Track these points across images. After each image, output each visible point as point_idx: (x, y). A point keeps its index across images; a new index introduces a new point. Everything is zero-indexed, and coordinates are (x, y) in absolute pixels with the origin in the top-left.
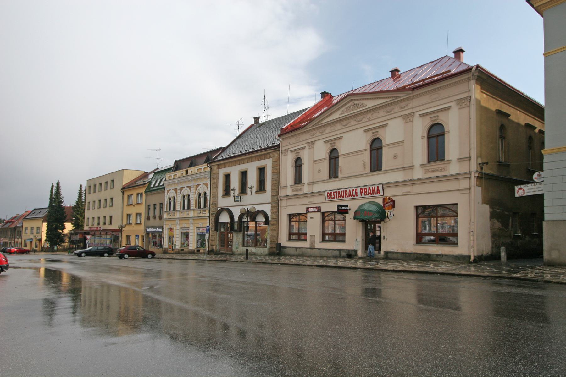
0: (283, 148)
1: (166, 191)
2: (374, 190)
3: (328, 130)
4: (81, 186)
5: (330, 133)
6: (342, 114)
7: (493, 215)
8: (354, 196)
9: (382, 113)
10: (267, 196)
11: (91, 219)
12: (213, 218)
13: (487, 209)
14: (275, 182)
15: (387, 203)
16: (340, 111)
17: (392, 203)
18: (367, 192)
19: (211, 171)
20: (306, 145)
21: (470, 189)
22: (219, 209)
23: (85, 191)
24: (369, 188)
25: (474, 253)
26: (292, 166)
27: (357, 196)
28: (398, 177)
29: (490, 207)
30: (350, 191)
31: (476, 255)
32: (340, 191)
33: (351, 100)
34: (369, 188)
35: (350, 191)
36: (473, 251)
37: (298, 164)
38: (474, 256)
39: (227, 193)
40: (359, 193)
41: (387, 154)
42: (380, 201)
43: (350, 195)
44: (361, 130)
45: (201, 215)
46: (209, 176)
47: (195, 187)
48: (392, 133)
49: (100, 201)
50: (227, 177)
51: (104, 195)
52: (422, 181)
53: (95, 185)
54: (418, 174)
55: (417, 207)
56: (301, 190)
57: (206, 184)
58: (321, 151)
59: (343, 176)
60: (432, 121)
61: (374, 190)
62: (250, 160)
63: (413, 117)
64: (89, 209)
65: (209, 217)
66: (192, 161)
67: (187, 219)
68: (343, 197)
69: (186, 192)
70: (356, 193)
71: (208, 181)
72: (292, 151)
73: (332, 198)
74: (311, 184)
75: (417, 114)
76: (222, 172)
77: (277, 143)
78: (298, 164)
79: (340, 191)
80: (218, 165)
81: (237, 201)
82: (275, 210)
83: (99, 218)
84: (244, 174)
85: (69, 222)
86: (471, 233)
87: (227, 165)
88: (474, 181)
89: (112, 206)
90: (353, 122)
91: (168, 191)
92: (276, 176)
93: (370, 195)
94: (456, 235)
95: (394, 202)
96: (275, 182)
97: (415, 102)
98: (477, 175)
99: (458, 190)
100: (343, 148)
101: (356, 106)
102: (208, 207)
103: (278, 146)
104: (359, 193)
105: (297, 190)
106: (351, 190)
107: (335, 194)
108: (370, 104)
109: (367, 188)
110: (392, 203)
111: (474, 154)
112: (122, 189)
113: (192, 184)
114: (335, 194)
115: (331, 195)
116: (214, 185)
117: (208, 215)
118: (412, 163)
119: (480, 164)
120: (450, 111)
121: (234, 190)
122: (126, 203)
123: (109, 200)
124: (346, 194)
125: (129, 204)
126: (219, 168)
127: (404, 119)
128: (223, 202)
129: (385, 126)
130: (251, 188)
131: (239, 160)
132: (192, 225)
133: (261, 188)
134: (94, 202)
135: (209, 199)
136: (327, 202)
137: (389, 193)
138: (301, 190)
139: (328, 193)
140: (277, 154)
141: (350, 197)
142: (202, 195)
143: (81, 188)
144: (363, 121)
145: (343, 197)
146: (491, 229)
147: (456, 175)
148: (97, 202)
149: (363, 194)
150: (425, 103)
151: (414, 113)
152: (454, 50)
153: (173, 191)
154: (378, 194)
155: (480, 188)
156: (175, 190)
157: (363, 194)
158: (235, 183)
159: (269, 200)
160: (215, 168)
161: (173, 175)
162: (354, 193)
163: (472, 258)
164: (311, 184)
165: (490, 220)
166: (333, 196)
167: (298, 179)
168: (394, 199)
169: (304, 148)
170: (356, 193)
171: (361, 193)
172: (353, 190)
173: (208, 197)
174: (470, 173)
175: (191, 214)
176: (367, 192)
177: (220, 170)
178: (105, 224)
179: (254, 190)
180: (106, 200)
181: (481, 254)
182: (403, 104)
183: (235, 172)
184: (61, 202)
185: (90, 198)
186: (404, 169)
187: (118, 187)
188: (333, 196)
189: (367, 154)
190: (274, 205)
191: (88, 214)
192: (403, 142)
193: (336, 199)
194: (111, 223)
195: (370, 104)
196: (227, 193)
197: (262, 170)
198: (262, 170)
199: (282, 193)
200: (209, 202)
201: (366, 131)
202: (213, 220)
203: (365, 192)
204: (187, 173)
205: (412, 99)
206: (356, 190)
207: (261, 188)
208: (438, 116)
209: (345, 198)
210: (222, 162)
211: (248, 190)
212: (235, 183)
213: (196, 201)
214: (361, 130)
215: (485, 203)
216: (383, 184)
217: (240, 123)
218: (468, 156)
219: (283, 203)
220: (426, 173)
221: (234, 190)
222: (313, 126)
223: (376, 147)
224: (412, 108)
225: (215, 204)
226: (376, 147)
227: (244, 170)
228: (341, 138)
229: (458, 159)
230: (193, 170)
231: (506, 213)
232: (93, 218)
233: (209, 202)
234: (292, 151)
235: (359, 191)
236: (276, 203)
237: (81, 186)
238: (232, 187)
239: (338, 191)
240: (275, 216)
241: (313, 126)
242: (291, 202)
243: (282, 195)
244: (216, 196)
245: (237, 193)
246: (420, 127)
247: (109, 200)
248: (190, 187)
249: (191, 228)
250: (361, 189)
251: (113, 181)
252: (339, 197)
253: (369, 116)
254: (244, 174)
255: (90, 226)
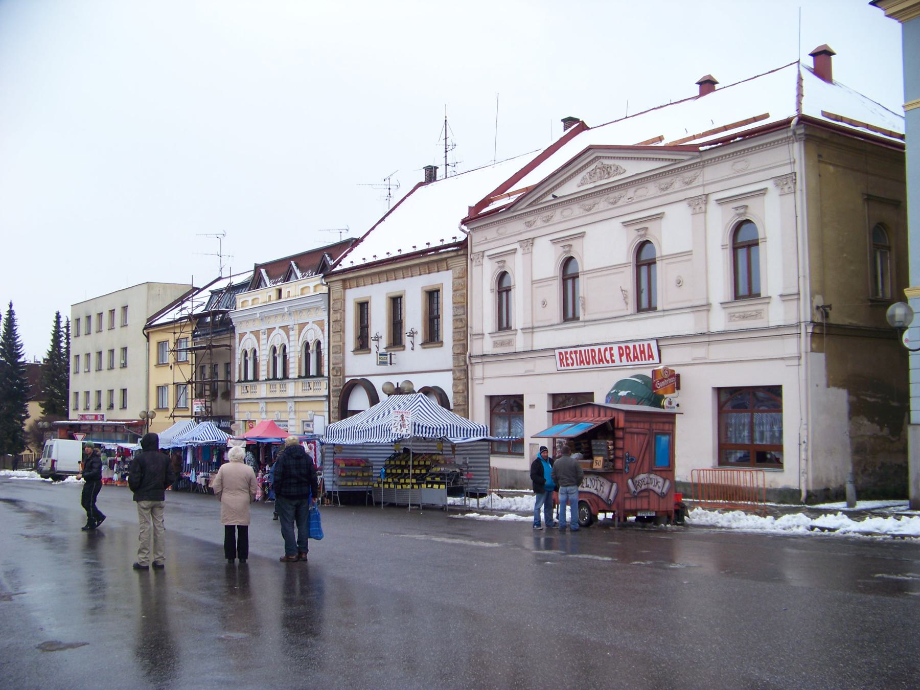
0: (475, 248)
1: (237, 336)
2: (642, 352)
3: (558, 215)
4: (58, 316)
5: (564, 221)
6: (583, 184)
7: (856, 410)
8: (608, 362)
9: (652, 189)
10: (443, 355)
11: (82, 397)
12: (335, 401)
13: (841, 397)
14: (460, 325)
15: (661, 381)
16: (578, 179)
17: (672, 380)
18: (631, 355)
19: (329, 294)
20: (517, 246)
21: (799, 358)
22: (347, 380)
23: (67, 327)
24: (634, 347)
25: (807, 485)
26: (492, 290)
27: (613, 361)
28: (684, 324)
29: (850, 393)
30: (599, 350)
31: (811, 488)
32: (596, 348)
33: (598, 158)
34: (634, 347)
35: (599, 350)
36: (807, 481)
37: (503, 287)
38: (808, 492)
39: (363, 344)
40: (616, 357)
41: (664, 274)
42: (650, 375)
43: (601, 360)
44: (617, 223)
45: (311, 393)
46: (323, 305)
47: (297, 327)
48: (674, 232)
49: (100, 353)
50: (363, 307)
51: (107, 340)
52: (725, 336)
53: (90, 319)
54: (718, 321)
55: (719, 391)
56: (509, 343)
57: (320, 323)
58: (546, 260)
59: (587, 318)
60: (738, 214)
61: (642, 352)
62: (408, 271)
63: (706, 202)
64: (77, 372)
65: (328, 397)
66: (281, 270)
67: (284, 400)
68: (588, 363)
69: (278, 338)
70: (612, 355)
71: (324, 316)
72: (491, 257)
73: (568, 365)
74: (530, 330)
75: (713, 197)
76: (354, 295)
77: (461, 237)
78: (503, 287)
79: (582, 349)
80: (344, 281)
81: (383, 363)
82: (461, 388)
83: (99, 392)
84: (396, 302)
85: (35, 400)
86: (803, 446)
87: (361, 281)
88: (805, 342)
89: (124, 366)
90: (602, 203)
91: (242, 335)
92: (461, 311)
93: (636, 362)
94: (780, 448)
95: (678, 376)
96: (460, 325)
97: (710, 173)
98: (810, 330)
99: (782, 359)
100: (589, 257)
101: (607, 171)
102: (326, 374)
103: (462, 246)
104: (616, 357)
105: (502, 344)
106: (603, 348)
107: (573, 356)
108: (632, 168)
109: (631, 345)
110: (672, 380)
111: (805, 289)
112: (145, 328)
113: (289, 322)
114: (573, 356)
115: (567, 359)
116: (335, 326)
117: (326, 393)
118: (707, 298)
119: (818, 308)
120: (767, 198)
121: (377, 339)
122: (153, 361)
123: (118, 353)
124: (593, 358)
125: (160, 364)
126: (345, 288)
127: (690, 205)
128: (358, 366)
129: (660, 216)
130: (412, 334)
131: (386, 272)
132: (292, 415)
133: (432, 337)
134: (88, 355)
135: (326, 358)
136: (559, 372)
137: (672, 358)
138: (509, 343)
139: (560, 353)
140: (459, 263)
141: (601, 365)
142: (312, 347)
143: (58, 322)
144: (620, 203)
145: (588, 363)
146: (851, 438)
147: (778, 327)
148: (94, 357)
149: (624, 358)
150: (722, 178)
151: (707, 195)
152: (811, 51)
153: (252, 336)
154: (651, 361)
155: (822, 356)
156: (256, 334)
157: (624, 358)
158: (379, 323)
159: (450, 364)
160: (337, 287)
161: (250, 299)
162: (608, 357)
163: (804, 494)
164: (530, 330)
165: (850, 418)
166: (570, 361)
167: (503, 324)
168: (677, 371)
169: (763, 192)
170: (612, 355)
171: (621, 355)
172: (606, 350)
173: (325, 352)
174: (798, 325)
175: (291, 389)
176: (631, 355)
177: (348, 291)
178: (111, 406)
179: (419, 339)
180: (112, 351)
181: (823, 487)
182: (688, 175)
183: (378, 295)
184: (176, 489)
185: (78, 346)
186: (694, 308)
187: (137, 320)
188: (570, 361)
189: (630, 272)
190: (458, 374)
191: (78, 383)
192: (689, 253)
193: (575, 366)
194: (124, 407)
195: (632, 168)
196: (363, 344)
197: (432, 296)
198: (432, 296)
199: (476, 347)
200: (326, 363)
201: (626, 224)
202: (336, 405)
203: (628, 355)
204: (280, 297)
205: (704, 166)
206: (611, 349)
207: (432, 337)
208: (746, 207)
209: (591, 365)
210: (351, 275)
211: (407, 341)
212: (379, 323)
213: (300, 360)
214: (617, 223)
215: (835, 385)
216: (658, 340)
217: (393, 181)
218: (796, 291)
219: (477, 371)
220: (730, 321)
221: (377, 339)
222: (530, 205)
223: (644, 259)
224: (704, 185)
225: (340, 370)
226: (644, 259)
227: (398, 294)
228: (582, 235)
229: (781, 296)
230: (292, 289)
231: (895, 404)
232: (88, 393)
233: (326, 363)
234: (491, 257)
235: (615, 352)
236: (462, 371)
237: (58, 316)
238: (372, 332)
239: (578, 349)
240: (460, 400)
241: (530, 205)
242: (492, 369)
243: (475, 353)
244: (341, 349)
245: (384, 343)
246: (719, 223)
247: (118, 353)
248: (286, 329)
249: (291, 422)
250: (620, 348)
251: (125, 308)
252: (582, 362)
253: (630, 193)
254: (396, 302)
255: (81, 412)
